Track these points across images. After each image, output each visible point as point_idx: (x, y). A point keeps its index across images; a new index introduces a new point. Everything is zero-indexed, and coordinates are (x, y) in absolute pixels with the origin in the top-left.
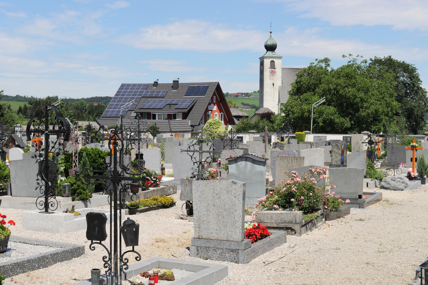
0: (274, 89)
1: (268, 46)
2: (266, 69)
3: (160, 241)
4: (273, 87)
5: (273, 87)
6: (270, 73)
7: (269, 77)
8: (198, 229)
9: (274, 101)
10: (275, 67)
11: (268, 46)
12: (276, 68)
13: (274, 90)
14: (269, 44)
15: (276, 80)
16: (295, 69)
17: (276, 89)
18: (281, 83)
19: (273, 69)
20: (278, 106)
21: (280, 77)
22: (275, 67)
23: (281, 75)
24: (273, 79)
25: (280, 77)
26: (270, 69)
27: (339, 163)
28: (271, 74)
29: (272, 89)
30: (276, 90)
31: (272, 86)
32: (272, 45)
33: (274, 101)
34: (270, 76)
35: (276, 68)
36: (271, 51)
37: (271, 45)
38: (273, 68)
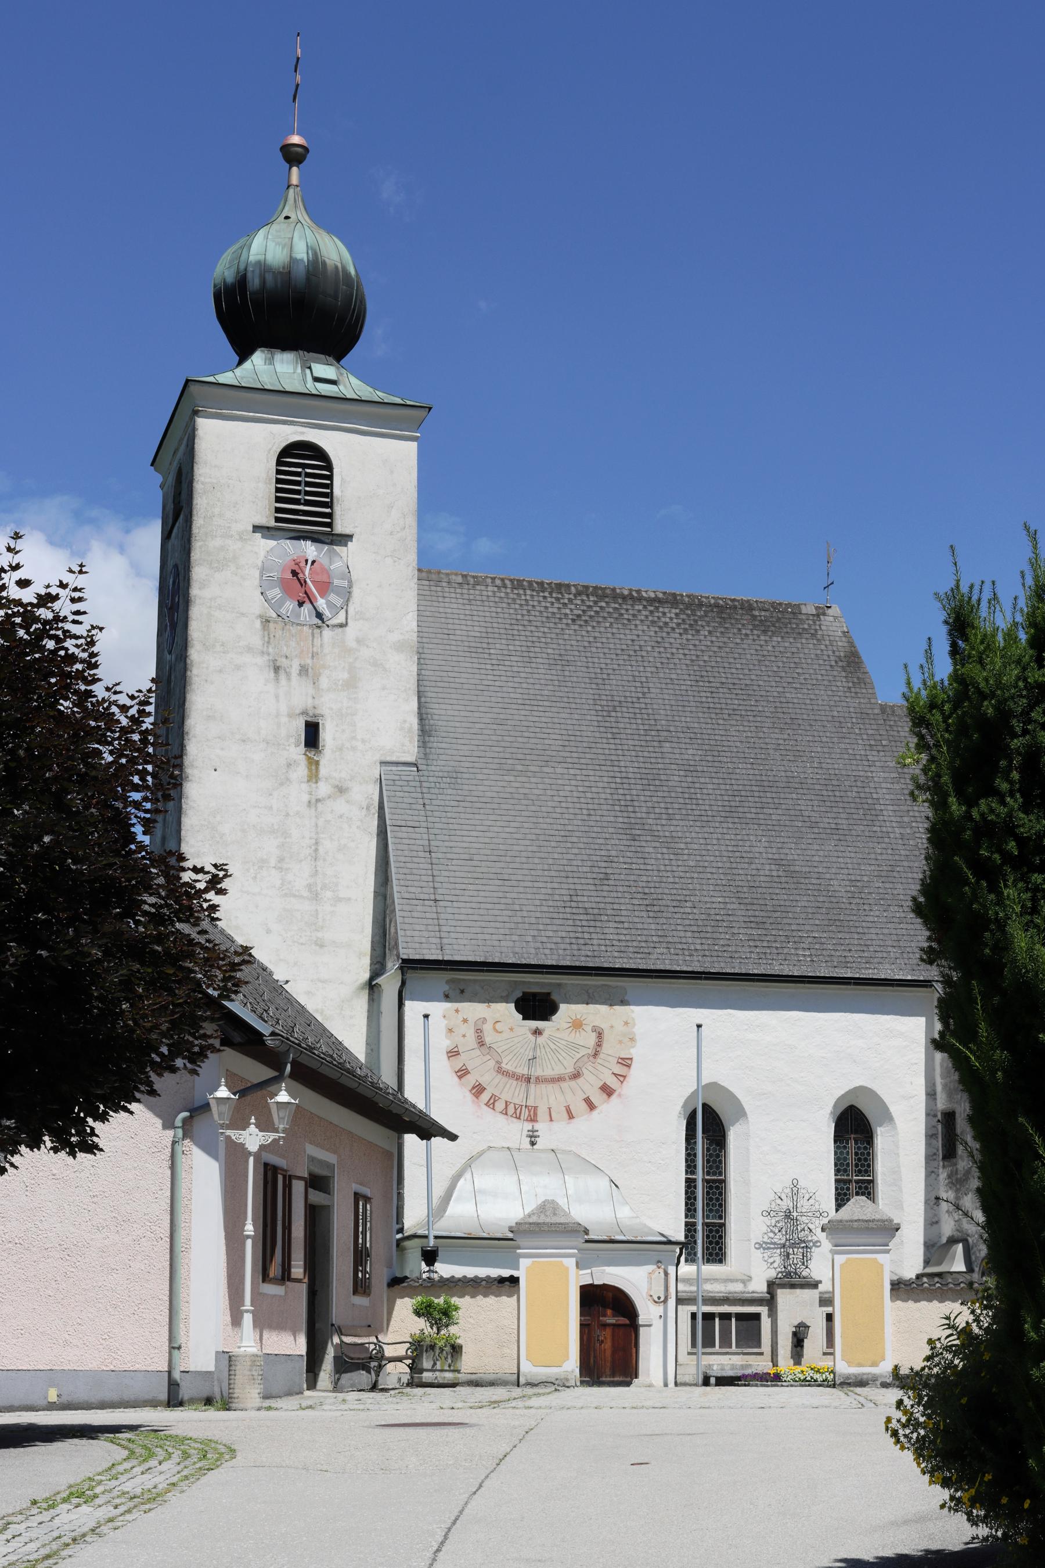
0: (323, 789)
1: (254, 283)
2: (215, 543)
3: (84, 1535)
4: (314, 765)
5: (314, 765)
6: (276, 593)
7: (256, 640)
8: (232, 1373)
9: (320, 944)
10: (340, 528)
11: (254, 283)
12: (344, 539)
13: (314, 803)
14: (263, 268)
15: (351, 684)
16: (584, 591)
17: (341, 790)
18: (414, 721)
19: (310, 550)
20: (362, 1003)
21: (399, 647)
22: (340, 528)
23: (410, 622)
24: (304, 670)
25: (399, 647)
26: (264, 545)
27: (164, 1396)
28: (276, 606)
29: (298, 792)
30: (340, 805)
31: (297, 751)
32: (300, 272)
33: (320, 944)
34: (266, 621)
35: (344, 539)
36: (285, 347)
37: (285, 274)
38: (315, 539)
